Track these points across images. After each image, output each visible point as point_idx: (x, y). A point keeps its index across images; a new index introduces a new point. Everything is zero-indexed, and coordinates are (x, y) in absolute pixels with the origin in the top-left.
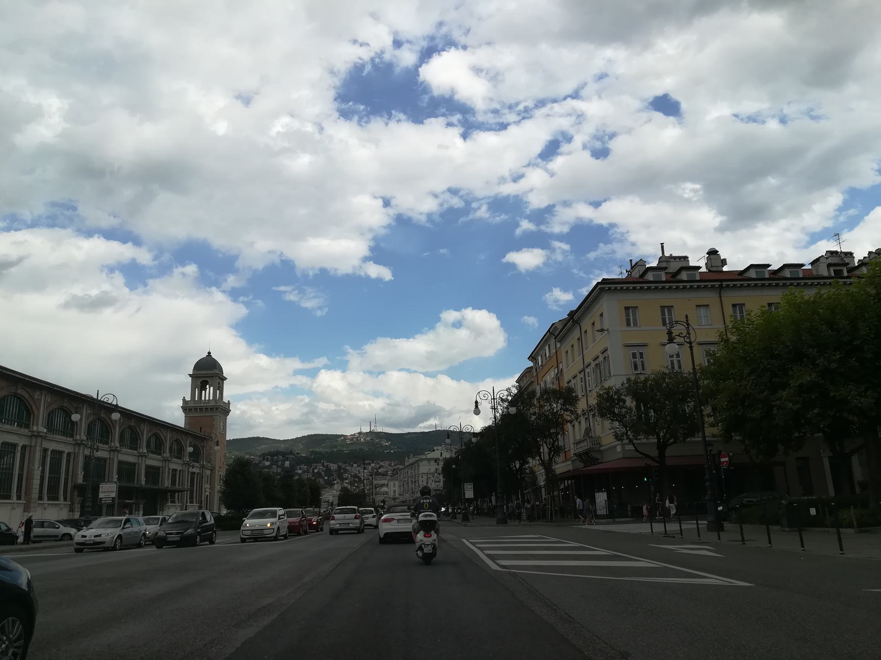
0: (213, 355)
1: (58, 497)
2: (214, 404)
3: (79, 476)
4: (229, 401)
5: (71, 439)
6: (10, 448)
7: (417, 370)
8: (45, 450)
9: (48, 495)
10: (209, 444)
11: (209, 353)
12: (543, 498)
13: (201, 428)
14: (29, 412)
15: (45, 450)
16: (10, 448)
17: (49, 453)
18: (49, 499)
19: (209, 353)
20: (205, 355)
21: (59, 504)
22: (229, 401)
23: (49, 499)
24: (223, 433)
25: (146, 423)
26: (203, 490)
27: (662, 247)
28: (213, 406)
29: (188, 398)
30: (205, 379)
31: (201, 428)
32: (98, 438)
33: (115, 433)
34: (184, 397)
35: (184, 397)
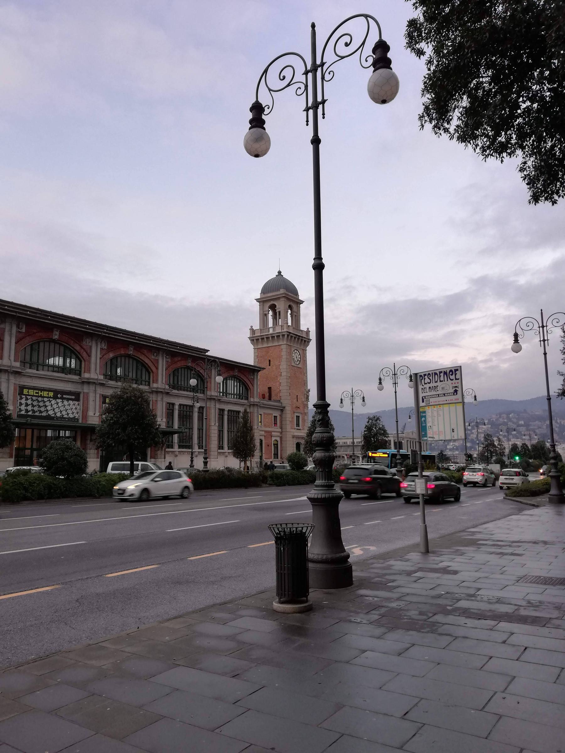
0: (285, 275)
1: (172, 445)
2: (280, 331)
3: (213, 428)
4: (308, 329)
5: (246, 401)
6: (233, 414)
7: (508, 584)
8: (222, 411)
9: (179, 444)
10: (279, 379)
11: (280, 272)
12: (234, 463)
13: (270, 361)
14: (148, 371)
15: (222, 411)
16: (233, 414)
17: (226, 413)
18: (180, 447)
19: (280, 272)
20: (274, 275)
21: (174, 451)
22: (308, 329)
23: (180, 447)
24: (299, 366)
25: (161, 352)
26: (23, 421)
27: (238, 675)
28: (279, 333)
29: (257, 326)
30: (272, 302)
31: (270, 361)
32: (244, 395)
33: (253, 390)
34: (252, 327)
35: (252, 327)
